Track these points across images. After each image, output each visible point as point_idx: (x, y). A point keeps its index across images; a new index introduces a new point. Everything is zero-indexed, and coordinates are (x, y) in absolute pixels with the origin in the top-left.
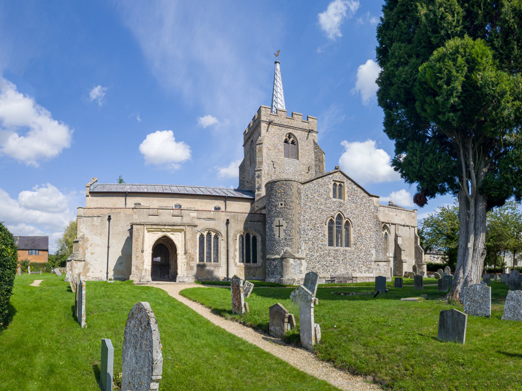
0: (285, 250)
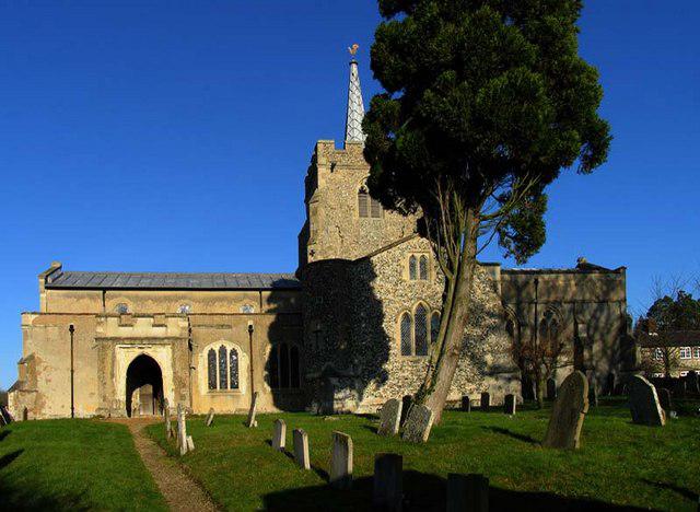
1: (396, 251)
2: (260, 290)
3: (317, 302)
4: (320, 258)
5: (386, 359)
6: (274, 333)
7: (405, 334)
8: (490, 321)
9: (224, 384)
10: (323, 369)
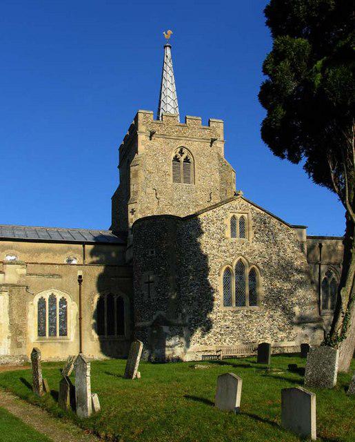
0: (157, 315)
1: (220, 211)
2: (84, 243)
3: (150, 254)
4: (140, 216)
5: (210, 309)
6: (102, 283)
7: (227, 286)
8: (298, 277)
9: (53, 332)
10: (154, 317)
